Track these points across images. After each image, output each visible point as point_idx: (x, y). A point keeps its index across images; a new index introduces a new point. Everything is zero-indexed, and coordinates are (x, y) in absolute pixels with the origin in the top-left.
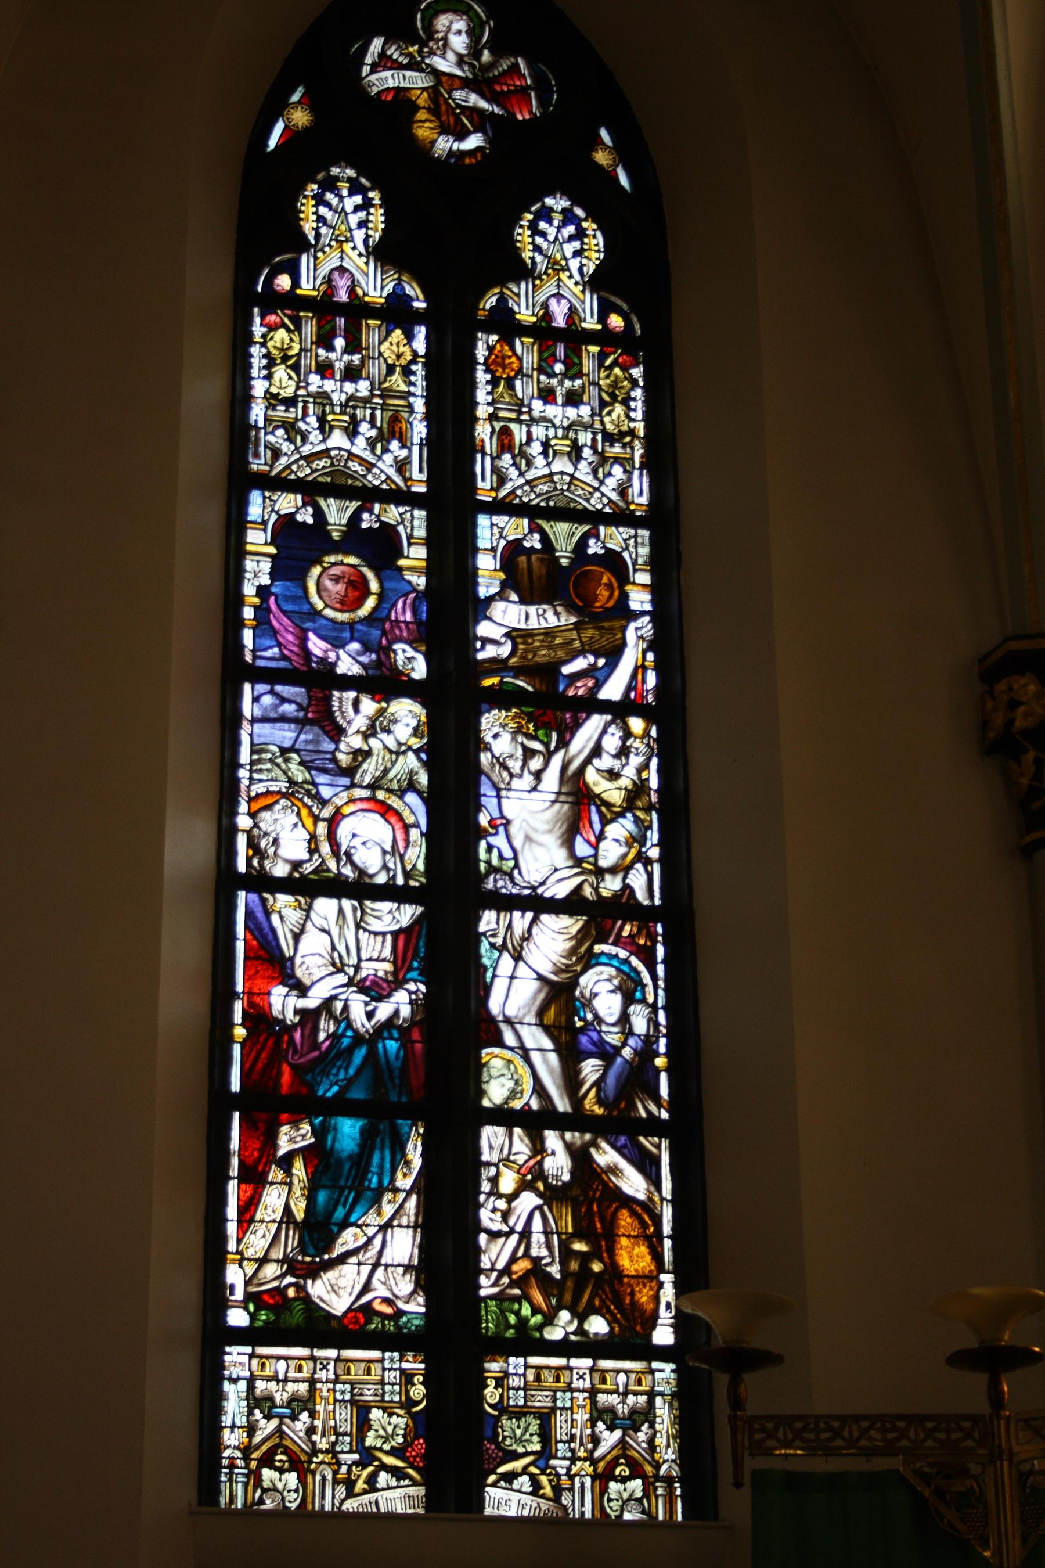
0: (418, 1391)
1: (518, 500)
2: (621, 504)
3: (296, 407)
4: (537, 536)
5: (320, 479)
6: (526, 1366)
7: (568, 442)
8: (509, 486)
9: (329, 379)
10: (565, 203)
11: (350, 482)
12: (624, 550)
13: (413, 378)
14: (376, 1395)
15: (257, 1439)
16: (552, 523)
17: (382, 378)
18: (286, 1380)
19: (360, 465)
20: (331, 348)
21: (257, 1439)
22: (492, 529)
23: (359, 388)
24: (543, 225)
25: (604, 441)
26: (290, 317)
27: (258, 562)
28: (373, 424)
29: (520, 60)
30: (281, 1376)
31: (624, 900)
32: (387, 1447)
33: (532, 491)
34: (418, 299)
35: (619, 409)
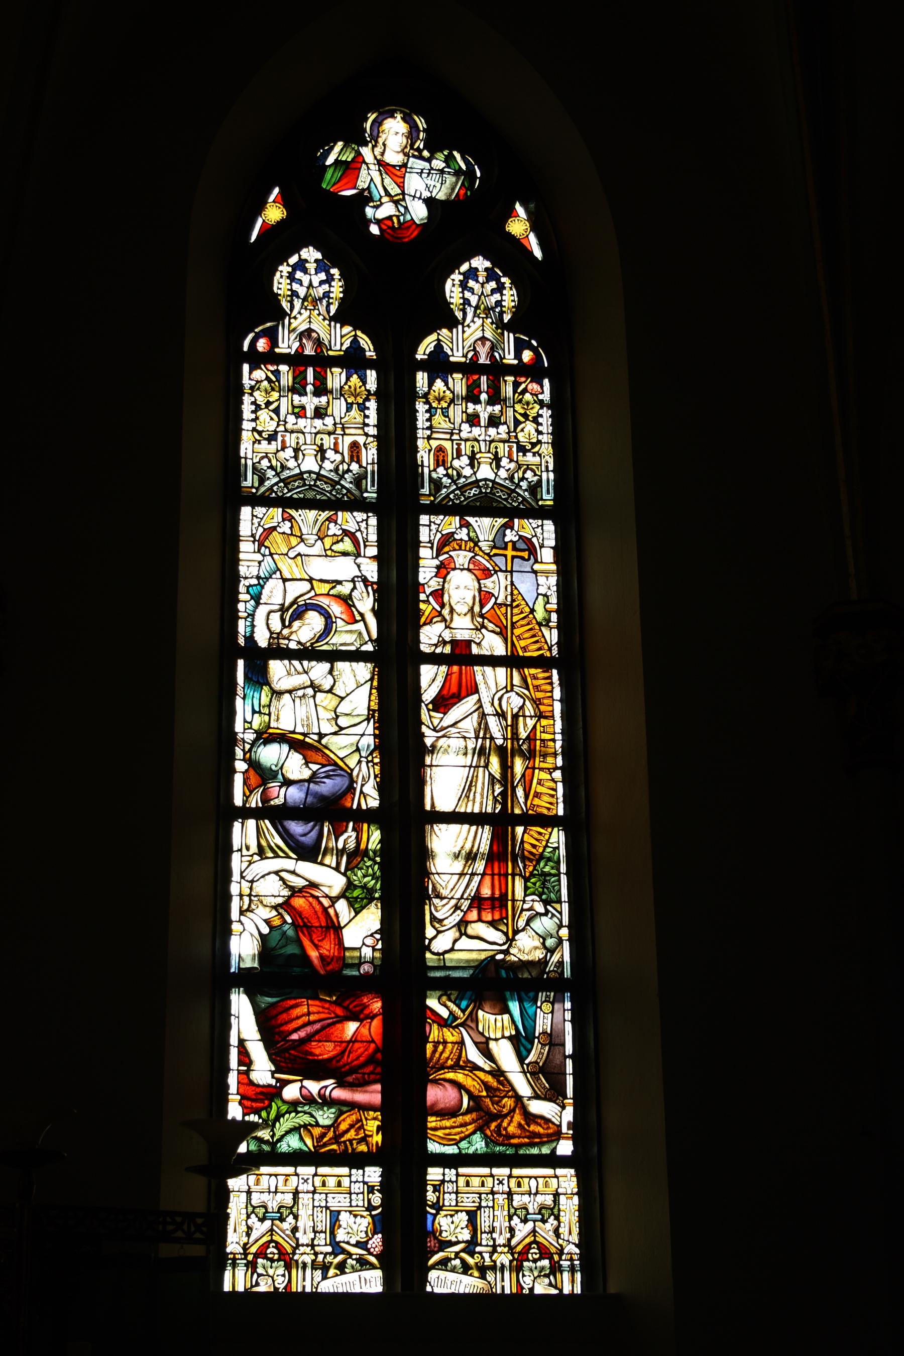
0: (376, 1199)
1: (274, 495)
2: (356, 493)
3: (276, 440)
5: (295, 496)
6: (458, 1175)
7: (490, 455)
8: (268, 484)
9: (476, 426)
10: (488, 264)
11: (495, 504)
13: (367, 412)
14: (474, 1202)
15: (252, 1239)
16: (477, 519)
17: (343, 416)
18: (276, 1192)
19: (502, 491)
20: (477, 401)
21: (252, 1239)
24: (471, 283)
26: (272, 372)
27: (547, 577)
29: (455, 153)
30: (533, 1191)
32: (353, 1242)
33: (462, 494)
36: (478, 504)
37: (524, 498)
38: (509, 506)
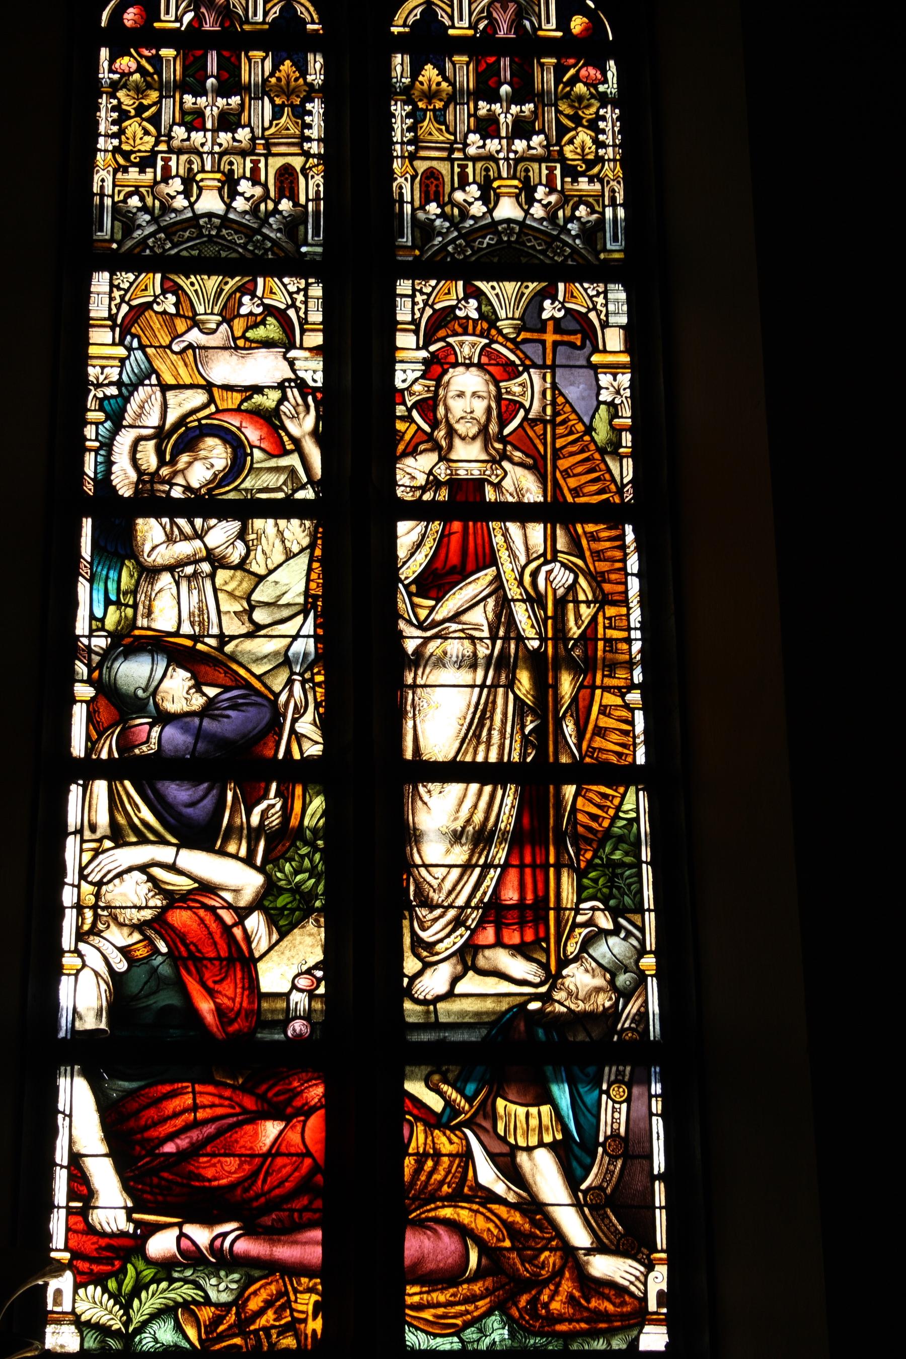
2: (289, 246)
3: (154, 166)
4: (473, 303)
11: (524, 260)
12: (590, 310)
17: (267, 124)
19: (536, 238)
20: (494, 98)
22: (111, 292)
23: (532, 144)
25: (563, 177)
26: (148, 59)
27: (103, 368)
28: (552, 190)
31: (299, 790)
34: (313, 22)
35: (584, 137)
36: (496, 260)
37: (574, 249)
38: (548, 261)
